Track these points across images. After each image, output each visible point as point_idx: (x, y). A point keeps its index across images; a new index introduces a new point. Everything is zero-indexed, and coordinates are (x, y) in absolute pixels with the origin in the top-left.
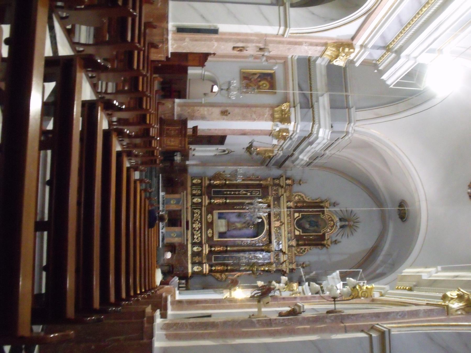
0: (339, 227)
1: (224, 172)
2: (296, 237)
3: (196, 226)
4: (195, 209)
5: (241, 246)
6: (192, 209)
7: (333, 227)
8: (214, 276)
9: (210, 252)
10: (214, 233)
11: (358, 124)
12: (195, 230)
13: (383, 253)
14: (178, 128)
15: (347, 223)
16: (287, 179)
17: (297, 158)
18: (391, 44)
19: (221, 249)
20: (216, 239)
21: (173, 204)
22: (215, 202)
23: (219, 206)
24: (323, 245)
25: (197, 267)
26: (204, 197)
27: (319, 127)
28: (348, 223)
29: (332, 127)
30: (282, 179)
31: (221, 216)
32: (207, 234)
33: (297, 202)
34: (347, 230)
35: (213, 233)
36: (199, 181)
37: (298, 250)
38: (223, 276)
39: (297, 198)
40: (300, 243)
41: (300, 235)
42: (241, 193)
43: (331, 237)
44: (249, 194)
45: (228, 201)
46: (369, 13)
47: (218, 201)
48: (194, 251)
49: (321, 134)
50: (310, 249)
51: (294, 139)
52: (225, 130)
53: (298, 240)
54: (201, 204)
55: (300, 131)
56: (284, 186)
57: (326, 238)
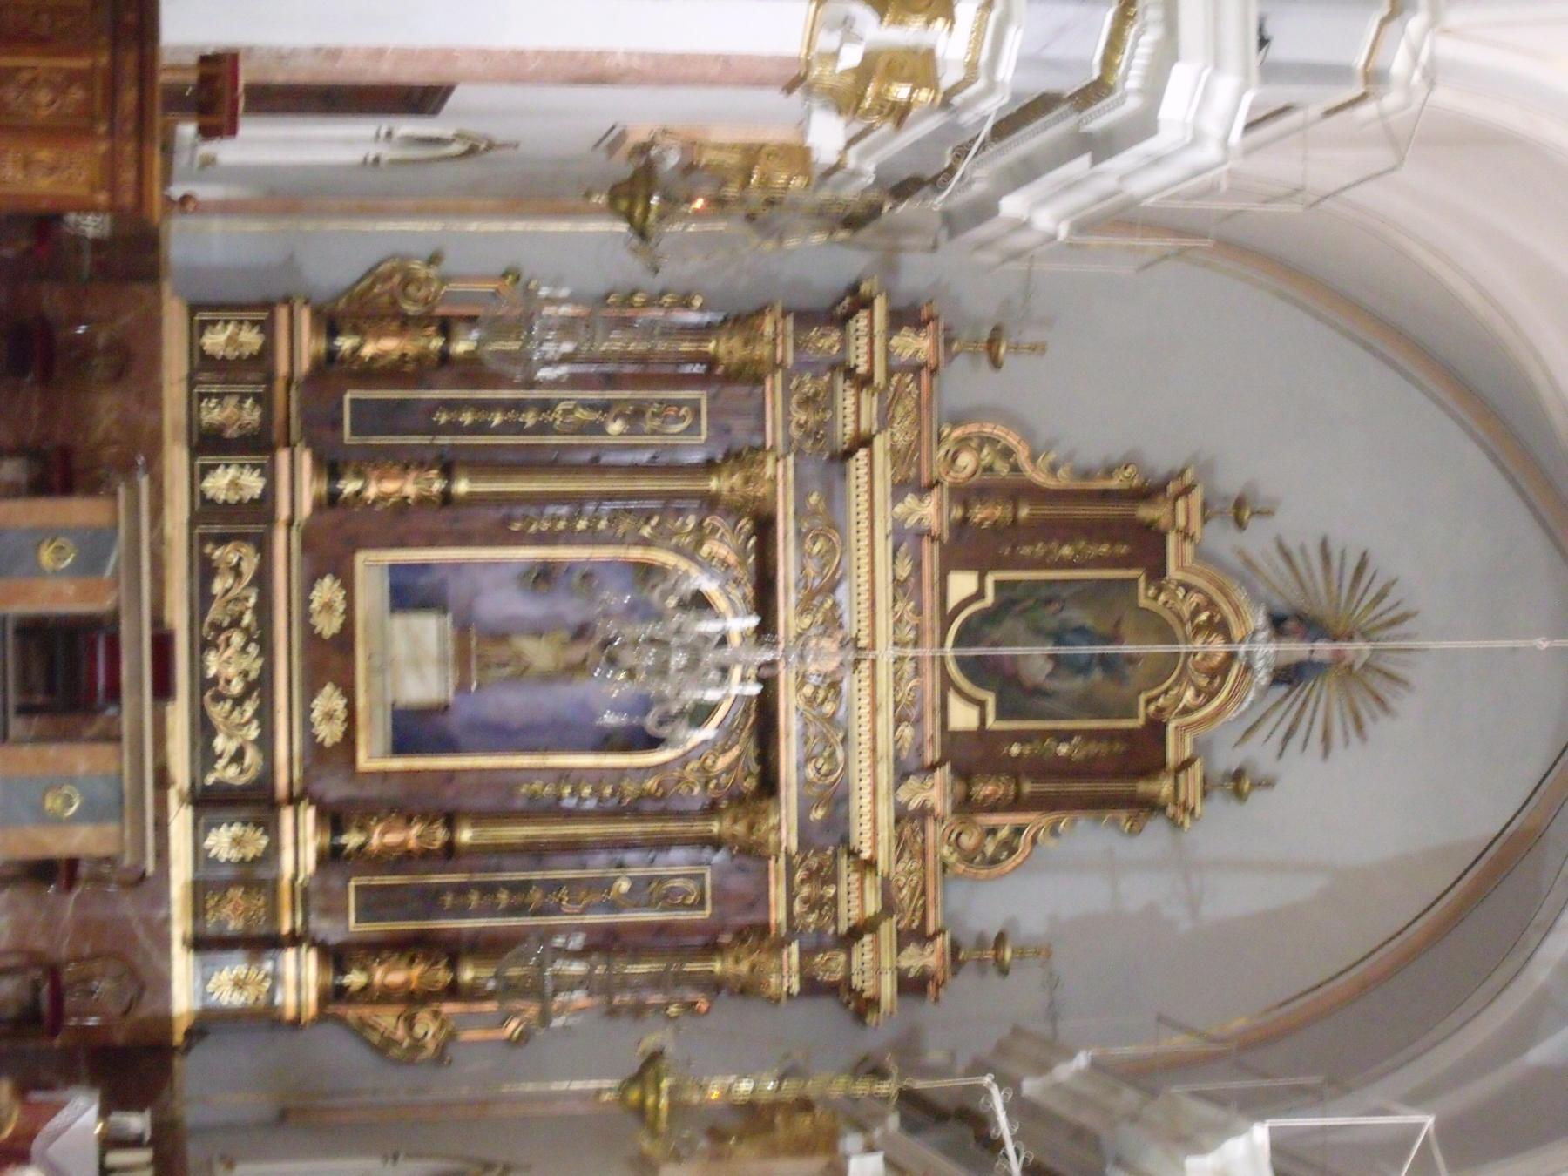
0: (1262, 677)
1: (434, 259)
2: (953, 741)
3: (229, 664)
4: (222, 540)
5: (553, 811)
6: (197, 542)
7: (1221, 671)
8: (360, 1030)
9: (331, 857)
10: (361, 718)
12: (219, 698)
14: (83, 63)
15: (1323, 649)
16: (905, 317)
17: (984, 210)
19: (413, 843)
20: (372, 756)
21: (56, 573)
22: (372, 492)
23: (399, 522)
24: (1151, 806)
25: (237, 829)
26: (283, 457)
27: (1168, 53)
28: (1328, 643)
29: (1263, 42)
30: (861, 321)
31: (408, 593)
32: (308, 725)
33: (965, 495)
34: (1324, 696)
35: (351, 718)
36: (251, 339)
37: (968, 841)
38: (426, 1026)
39: (966, 460)
40: (985, 790)
41: (982, 731)
42: (557, 417)
43: (1203, 749)
44: (616, 427)
45: (462, 487)
47: (390, 486)
48: (214, 862)
49: (1175, 109)
50: (1054, 831)
51: (967, 118)
52: (448, 55)
53: (964, 774)
54: (261, 509)
55: (1024, 62)
56: (879, 377)
57: (1172, 756)
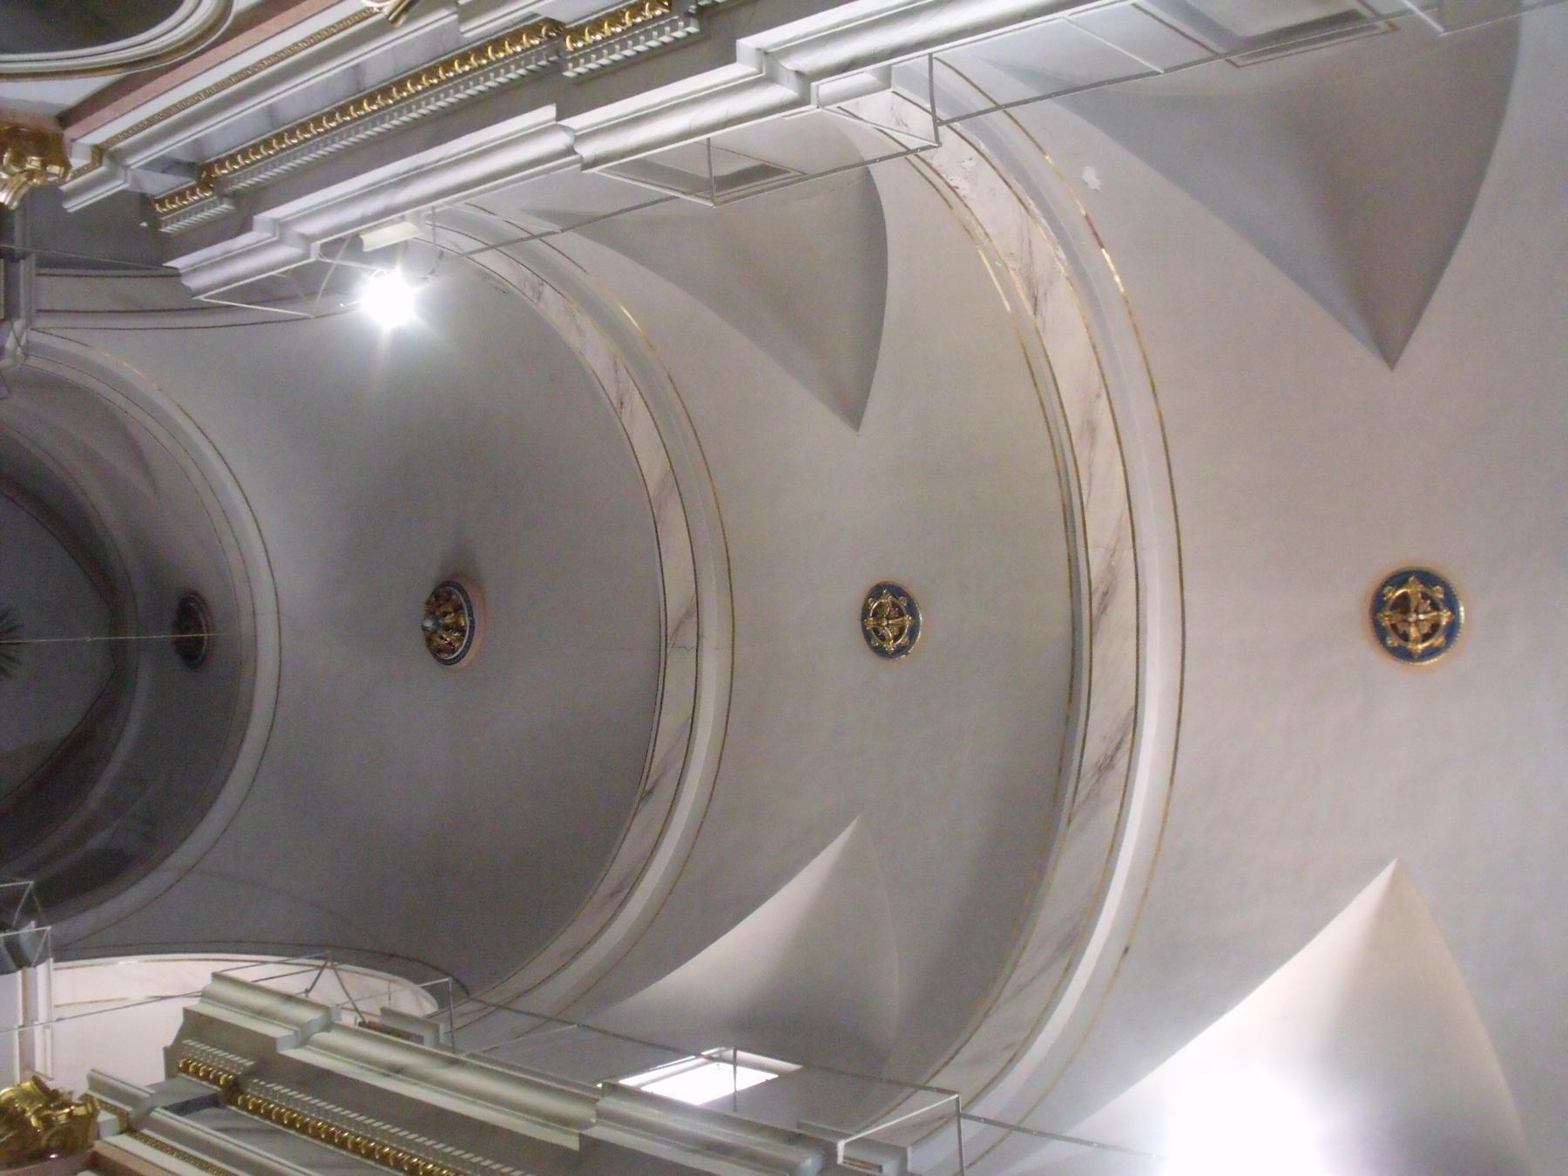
11: (42, 322)
13: (112, 771)
18: (221, 163)
46: (135, 78)
